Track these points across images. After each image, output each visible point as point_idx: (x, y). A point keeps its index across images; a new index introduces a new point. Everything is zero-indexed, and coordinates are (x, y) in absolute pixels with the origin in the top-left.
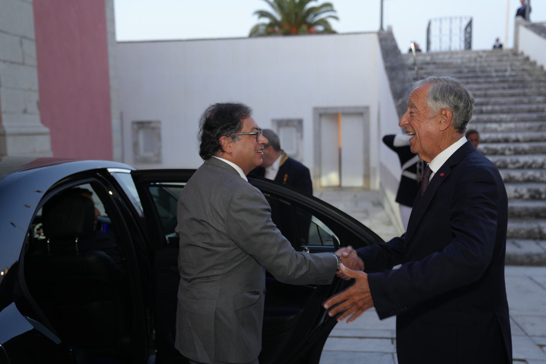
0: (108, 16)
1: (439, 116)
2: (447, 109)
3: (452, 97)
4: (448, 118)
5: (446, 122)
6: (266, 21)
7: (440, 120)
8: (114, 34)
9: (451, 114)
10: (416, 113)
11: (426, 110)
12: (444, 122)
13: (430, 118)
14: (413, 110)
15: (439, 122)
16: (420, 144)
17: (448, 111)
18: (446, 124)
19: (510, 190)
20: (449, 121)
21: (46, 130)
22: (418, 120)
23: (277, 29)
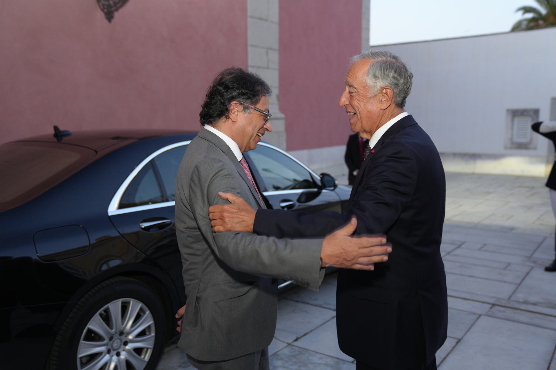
0: (364, 26)
1: (380, 95)
2: (388, 88)
3: (392, 74)
4: (389, 96)
5: (387, 100)
6: (530, 16)
7: (381, 99)
8: (368, 40)
9: (392, 92)
10: (356, 93)
11: (365, 89)
12: (385, 100)
13: (370, 98)
14: (352, 90)
15: (380, 101)
16: (361, 125)
17: (388, 89)
18: (388, 103)
19: (249, 178)
20: (390, 99)
21: (282, 116)
22: (358, 100)
23: (541, 22)
